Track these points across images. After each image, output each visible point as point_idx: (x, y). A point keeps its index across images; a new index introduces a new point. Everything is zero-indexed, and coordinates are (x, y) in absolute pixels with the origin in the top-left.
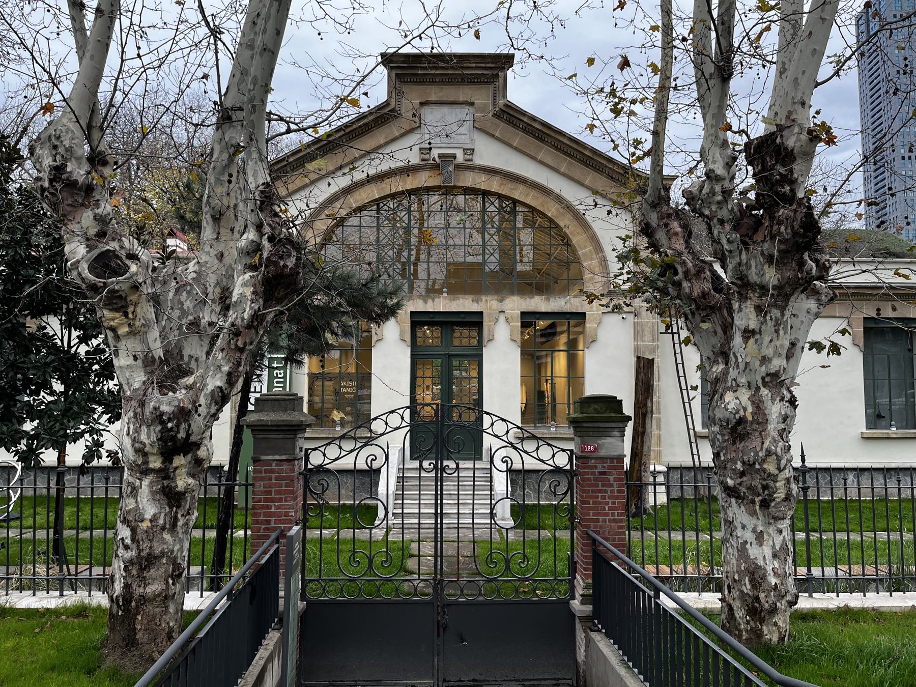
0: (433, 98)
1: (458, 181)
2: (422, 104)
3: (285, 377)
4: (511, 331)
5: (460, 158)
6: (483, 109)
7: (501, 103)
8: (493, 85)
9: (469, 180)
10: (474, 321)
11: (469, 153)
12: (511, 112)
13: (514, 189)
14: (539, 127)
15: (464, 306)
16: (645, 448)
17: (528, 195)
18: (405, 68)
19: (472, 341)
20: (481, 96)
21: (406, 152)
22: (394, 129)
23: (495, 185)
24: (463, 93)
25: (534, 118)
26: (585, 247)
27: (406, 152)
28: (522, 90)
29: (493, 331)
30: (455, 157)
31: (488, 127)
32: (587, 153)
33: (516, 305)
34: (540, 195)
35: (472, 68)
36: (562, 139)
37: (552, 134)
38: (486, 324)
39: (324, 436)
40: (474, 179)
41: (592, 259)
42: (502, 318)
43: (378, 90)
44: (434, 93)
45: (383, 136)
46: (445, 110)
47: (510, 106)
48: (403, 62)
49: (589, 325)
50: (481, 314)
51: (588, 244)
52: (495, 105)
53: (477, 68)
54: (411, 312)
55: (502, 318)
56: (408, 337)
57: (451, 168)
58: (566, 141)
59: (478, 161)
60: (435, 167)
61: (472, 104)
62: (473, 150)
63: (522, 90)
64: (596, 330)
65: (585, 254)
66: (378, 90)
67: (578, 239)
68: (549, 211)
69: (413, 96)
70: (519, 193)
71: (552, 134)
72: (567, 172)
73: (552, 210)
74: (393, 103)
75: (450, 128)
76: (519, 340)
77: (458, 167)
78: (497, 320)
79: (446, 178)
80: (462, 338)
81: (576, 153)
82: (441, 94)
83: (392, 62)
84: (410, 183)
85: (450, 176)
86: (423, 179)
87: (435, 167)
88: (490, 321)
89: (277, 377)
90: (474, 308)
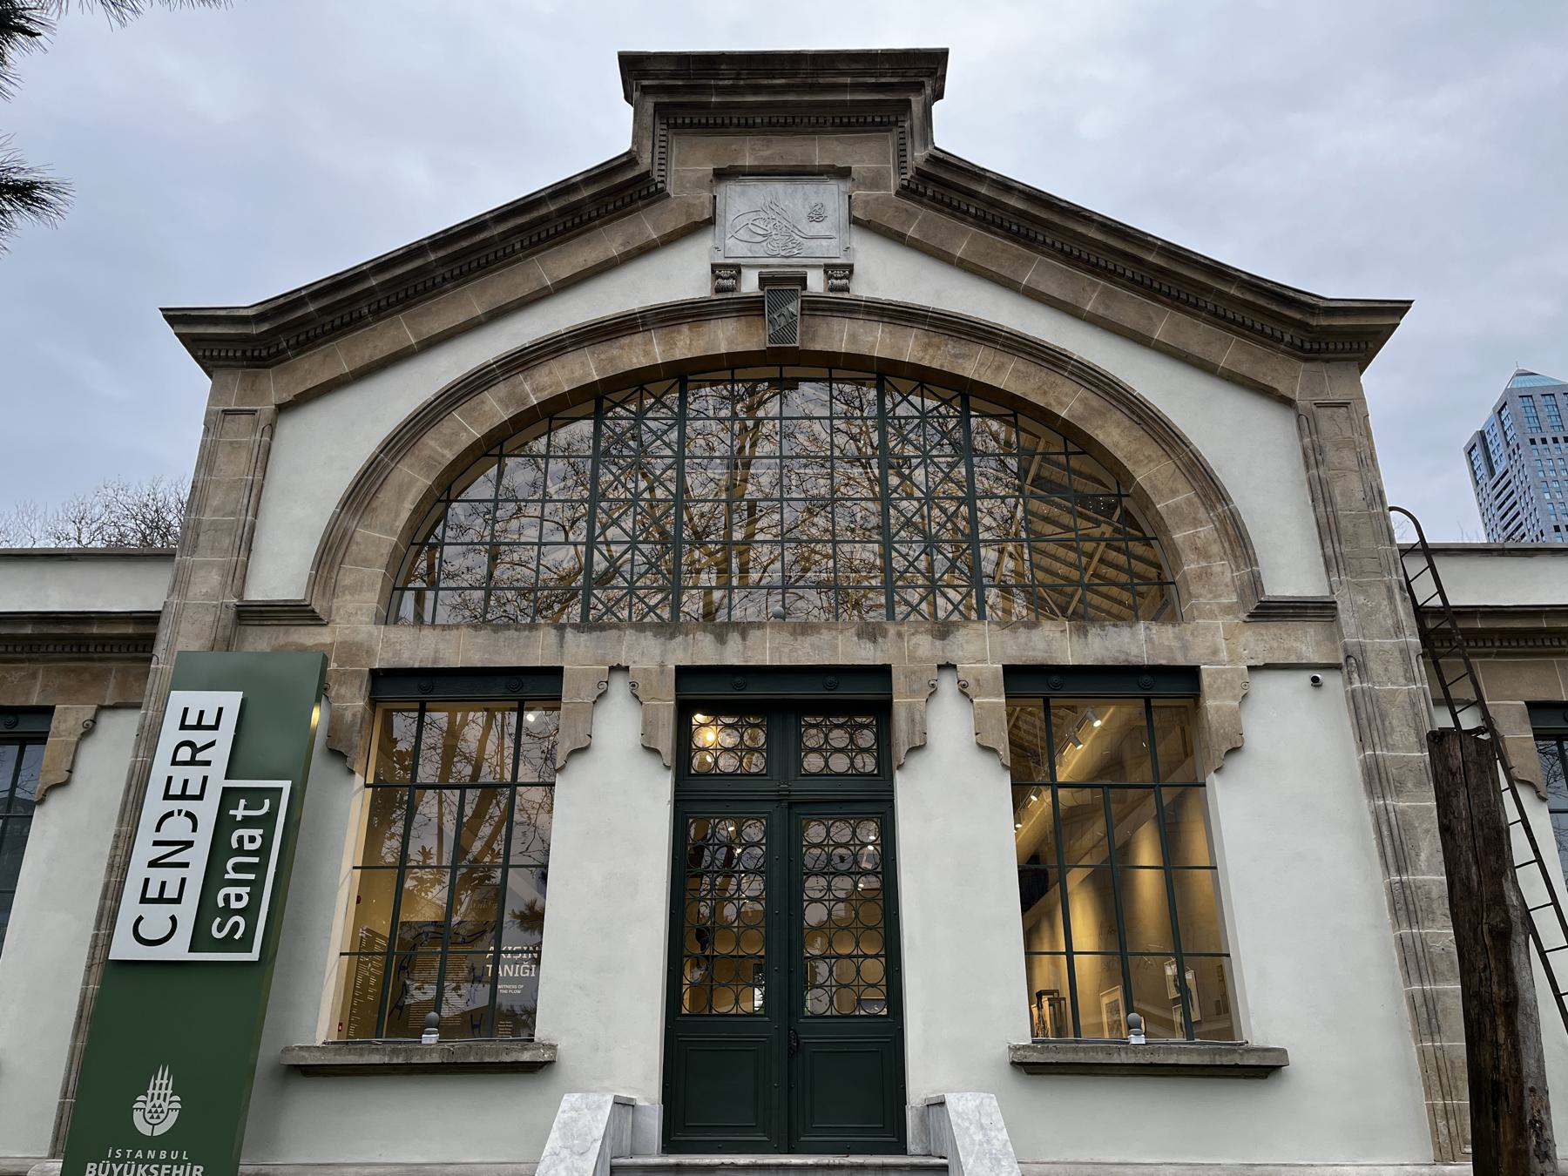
0: (748, 161)
1: (813, 340)
2: (722, 175)
3: (263, 852)
4: (979, 721)
5: (816, 283)
6: (875, 182)
7: (918, 155)
8: (896, 130)
9: (840, 337)
10: (863, 697)
11: (839, 273)
12: (946, 176)
13: (964, 356)
14: (1020, 205)
15: (834, 648)
16: (1529, 1064)
17: (999, 368)
18: (675, 89)
19: (859, 762)
20: (867, 156)
21: (680, 276)
22: (648, 226)
23: (910, 347)
24: (819, 152)
25: (1005, 185)
26: (1174, 493)
27: (680, 276)
28: (961, 127)
29: (923, 721)
30: (802, 281)
31: (887, 219)
32: (1151, 258)
33: (985, 649)
34: (1033, 369)
35: (842, 88)
36: (543, 211)
37: (1056, 219)
38: (899, 702)
39: (375, 1059)
40: (853, 338)
41: (1196, 522)
42: (947, 684)
43: (606, 129)
44: (749, 153)
45: (619, 241)
46: (778, 189)
47: (943, 161)
48: (674, 76)
49: (1214, 703)
50: (884, 672)
51: (1181, 484)
52: (901, 166)
53: (855, 87)
54: (680, 670)
55: (947, 684)
56: (666, 742)
57: (794, 307)
58: (1092, 233)
59: (861, 289)
60: (750, 308)
61: (843, 174)
62: (850, 267)
63: (961, 127)
64: (1235, 716)
65: (1176, 510)
66: (606, 129)
67: (1150, 470)
68: (1062, 405)
69: (687, 167)
70: (976, 365)
71: (1056, 219)
72: (1101, 311)
73: (1068, 402)
74: (645, 161)
75: (780, 222)
76: (1004, 747)
77: (814, 307)
78: (933, 692)
79: (779, 343)
80: (829, 752)
81: (1121, 265)
82: (767, 153)
83: (645, 74)
84: (686, 344)
85: (791, 326)
86: (724, 337)
87: (750, 308)
88: (913, 693)
89: (241, 851)
90: (865, 654)
